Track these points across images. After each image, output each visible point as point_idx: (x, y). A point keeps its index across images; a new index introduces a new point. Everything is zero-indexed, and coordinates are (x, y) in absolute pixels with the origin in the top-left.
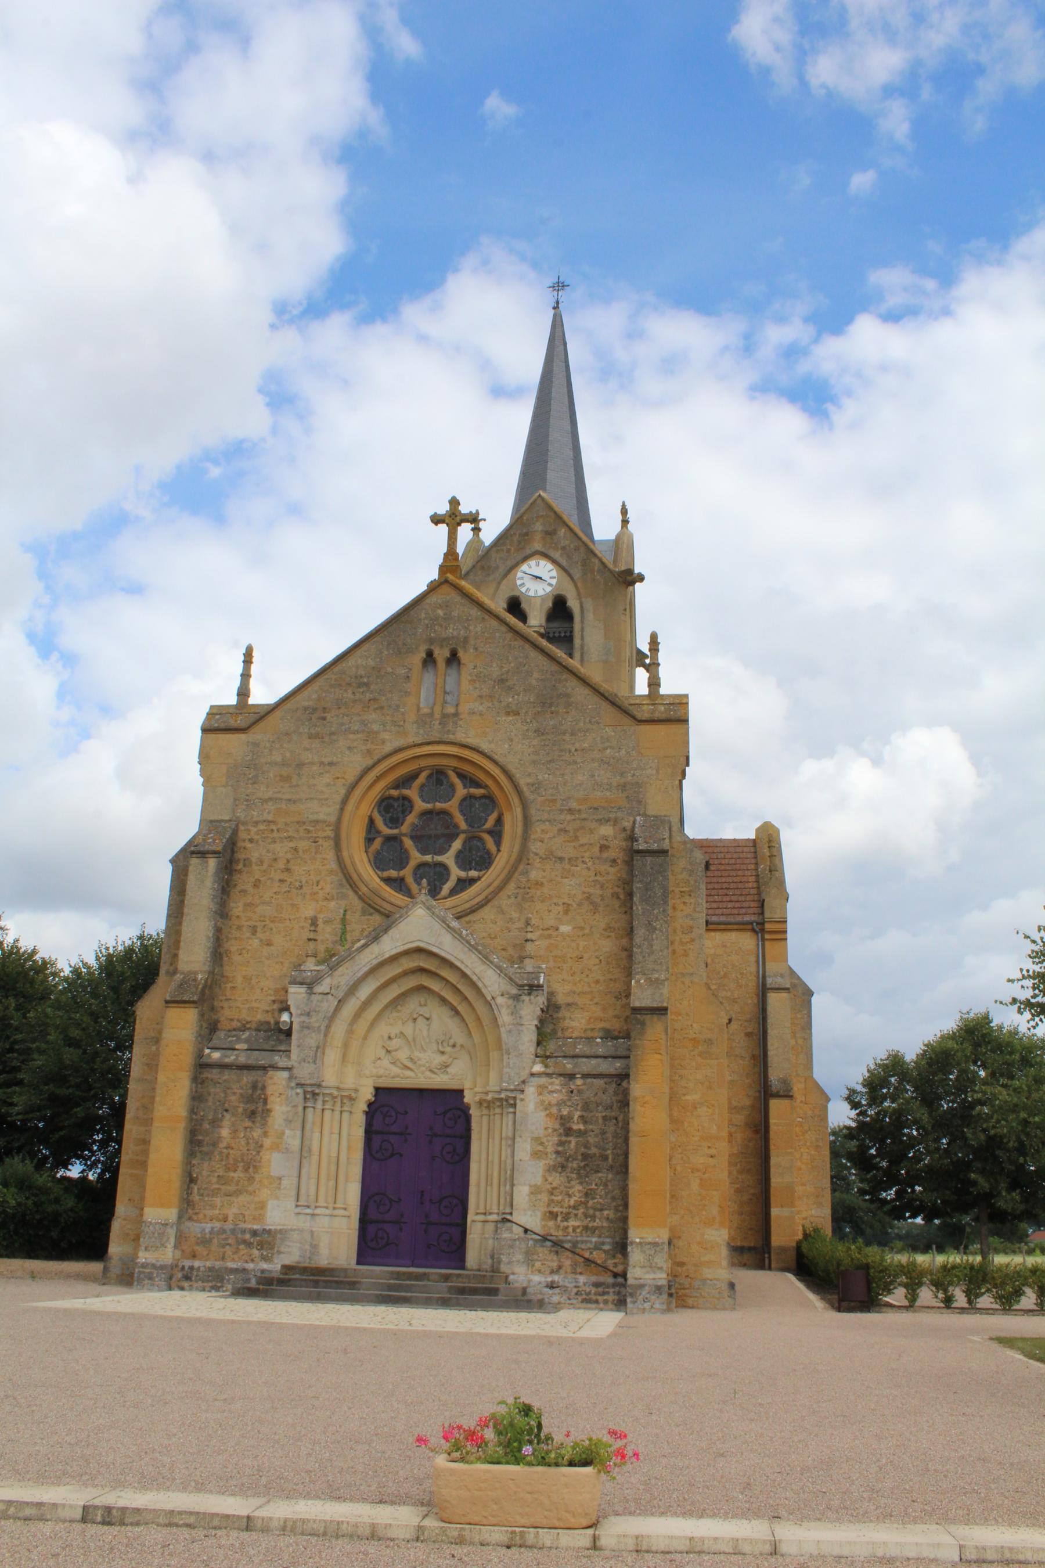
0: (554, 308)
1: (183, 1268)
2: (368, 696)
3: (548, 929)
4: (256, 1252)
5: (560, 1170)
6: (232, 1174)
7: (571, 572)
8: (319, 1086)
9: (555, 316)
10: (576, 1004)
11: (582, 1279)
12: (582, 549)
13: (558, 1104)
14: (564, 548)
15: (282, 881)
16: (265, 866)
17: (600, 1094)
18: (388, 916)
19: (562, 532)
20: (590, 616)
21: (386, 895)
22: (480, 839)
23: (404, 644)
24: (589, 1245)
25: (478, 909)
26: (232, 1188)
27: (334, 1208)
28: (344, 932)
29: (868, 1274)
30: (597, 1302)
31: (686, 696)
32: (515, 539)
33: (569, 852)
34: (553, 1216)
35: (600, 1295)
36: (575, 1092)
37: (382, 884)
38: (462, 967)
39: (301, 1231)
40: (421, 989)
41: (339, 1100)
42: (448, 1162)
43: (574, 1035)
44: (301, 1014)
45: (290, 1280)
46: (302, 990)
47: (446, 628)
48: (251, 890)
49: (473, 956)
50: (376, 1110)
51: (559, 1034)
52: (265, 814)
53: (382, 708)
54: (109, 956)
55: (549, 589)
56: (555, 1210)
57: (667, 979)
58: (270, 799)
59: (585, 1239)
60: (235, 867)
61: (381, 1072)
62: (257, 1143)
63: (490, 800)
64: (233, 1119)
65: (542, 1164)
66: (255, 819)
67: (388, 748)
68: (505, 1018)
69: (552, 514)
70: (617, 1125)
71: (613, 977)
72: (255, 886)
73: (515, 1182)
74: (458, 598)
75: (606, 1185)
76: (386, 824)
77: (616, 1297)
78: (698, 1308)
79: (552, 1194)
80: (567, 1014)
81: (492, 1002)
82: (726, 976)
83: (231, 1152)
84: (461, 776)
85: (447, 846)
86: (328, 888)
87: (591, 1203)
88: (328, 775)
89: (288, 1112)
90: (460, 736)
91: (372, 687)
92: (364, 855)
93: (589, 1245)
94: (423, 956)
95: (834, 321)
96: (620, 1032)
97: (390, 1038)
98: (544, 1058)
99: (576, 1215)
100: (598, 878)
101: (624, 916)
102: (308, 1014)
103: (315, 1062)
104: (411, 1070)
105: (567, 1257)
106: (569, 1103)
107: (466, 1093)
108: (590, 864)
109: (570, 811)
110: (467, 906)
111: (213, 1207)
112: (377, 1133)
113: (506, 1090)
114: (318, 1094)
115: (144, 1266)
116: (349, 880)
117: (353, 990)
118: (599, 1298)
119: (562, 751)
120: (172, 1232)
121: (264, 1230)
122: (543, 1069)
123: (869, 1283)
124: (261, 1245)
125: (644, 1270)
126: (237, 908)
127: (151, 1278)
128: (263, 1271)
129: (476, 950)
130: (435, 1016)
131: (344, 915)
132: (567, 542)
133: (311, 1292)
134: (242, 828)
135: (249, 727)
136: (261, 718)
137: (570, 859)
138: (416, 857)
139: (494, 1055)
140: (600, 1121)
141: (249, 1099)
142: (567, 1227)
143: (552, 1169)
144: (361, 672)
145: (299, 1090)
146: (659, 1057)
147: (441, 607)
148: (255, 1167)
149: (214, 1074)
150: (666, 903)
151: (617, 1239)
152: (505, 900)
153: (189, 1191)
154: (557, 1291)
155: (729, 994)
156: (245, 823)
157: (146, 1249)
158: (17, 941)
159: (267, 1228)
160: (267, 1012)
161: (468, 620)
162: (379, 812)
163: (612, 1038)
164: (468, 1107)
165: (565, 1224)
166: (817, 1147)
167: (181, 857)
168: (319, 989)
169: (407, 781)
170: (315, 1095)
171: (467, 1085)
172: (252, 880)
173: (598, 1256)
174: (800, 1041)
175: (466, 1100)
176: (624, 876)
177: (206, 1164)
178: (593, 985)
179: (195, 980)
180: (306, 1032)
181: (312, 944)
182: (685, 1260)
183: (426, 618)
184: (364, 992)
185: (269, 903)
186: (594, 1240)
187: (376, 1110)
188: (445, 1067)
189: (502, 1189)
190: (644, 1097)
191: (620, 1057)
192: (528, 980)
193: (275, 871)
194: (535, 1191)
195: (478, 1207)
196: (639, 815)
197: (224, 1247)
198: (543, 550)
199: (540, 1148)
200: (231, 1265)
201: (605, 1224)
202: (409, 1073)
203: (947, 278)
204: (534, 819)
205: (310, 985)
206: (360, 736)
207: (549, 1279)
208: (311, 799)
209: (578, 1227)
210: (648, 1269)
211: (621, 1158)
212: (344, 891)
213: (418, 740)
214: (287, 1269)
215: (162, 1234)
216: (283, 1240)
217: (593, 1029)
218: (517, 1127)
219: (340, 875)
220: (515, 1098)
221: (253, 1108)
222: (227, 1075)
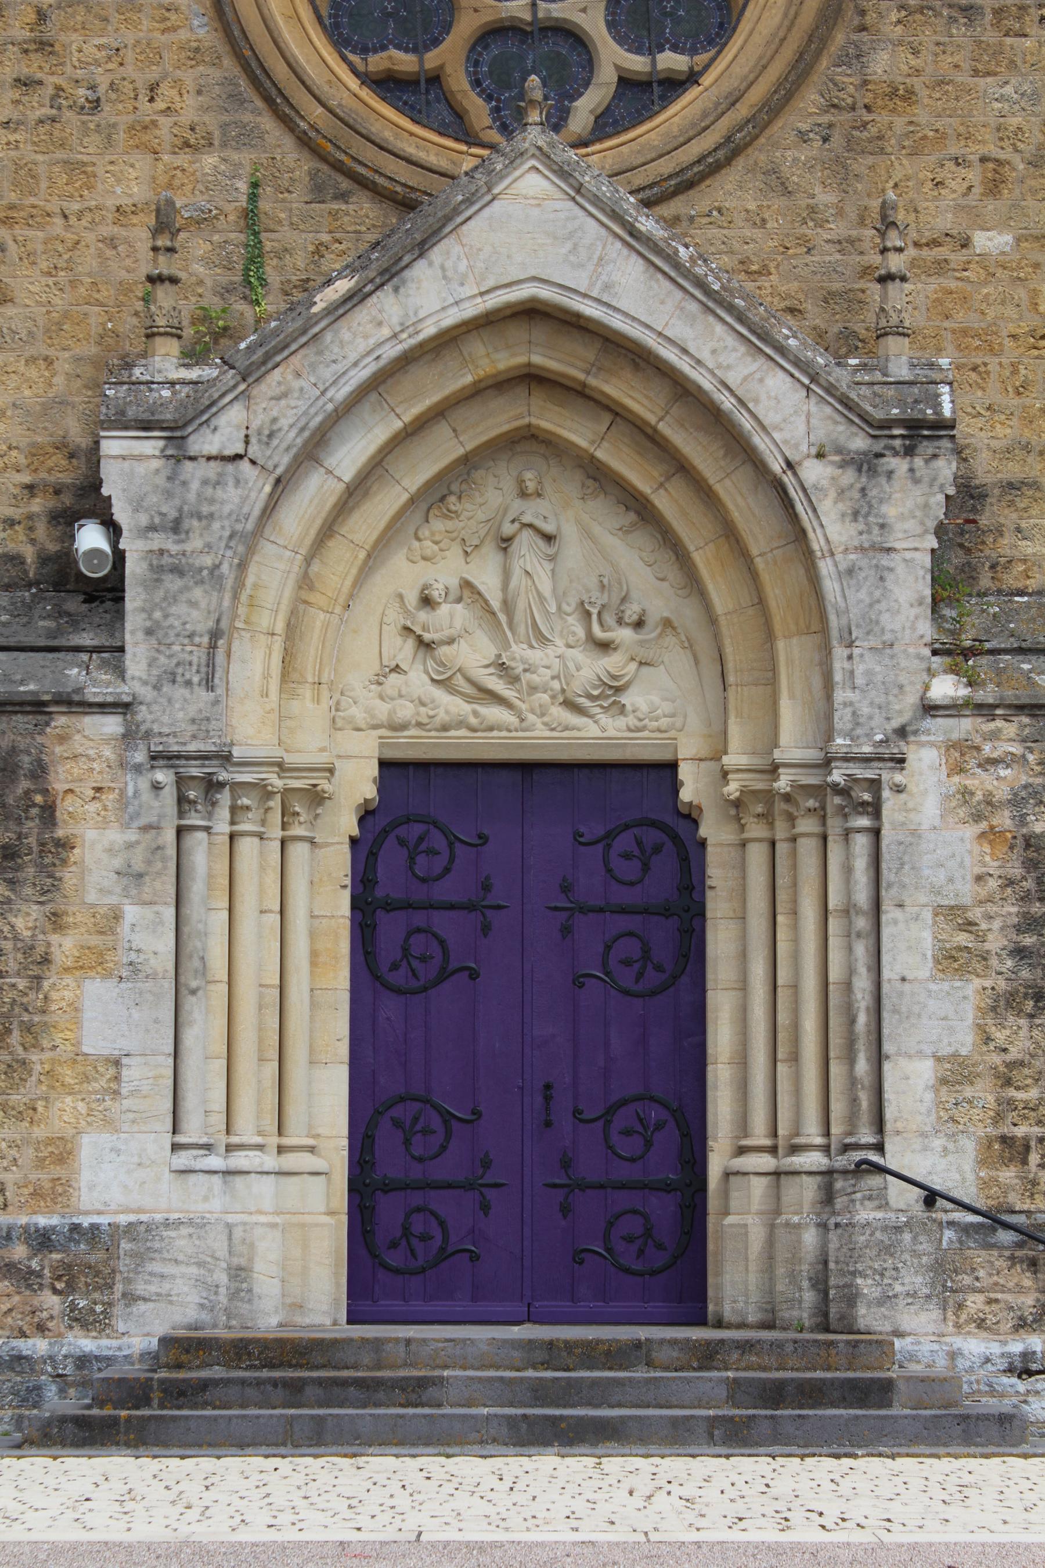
3: (934, 243)
4: (51, 1302)
5: (1029, 1005)
8: (225, 758)
13: (1016, 801)
15: (25, 83)
18: (406, 204)
21: (388, 135)
25: (703, 177)
27: (281, 1150)
28: (255, 258)
34: (1015, 1150)
37: (365, 93)
38: (684, 365)
39: (198, 1225)
41: (276, 803)
42: (626, 993)
43: (1032, 584)
44: (152, 528)
46: (151, 446)
49: (719, 329)
50: (385, 832)
51: (985, 581)
56: (1020, 1131)
61: (406, 711)
65: (971, 992)
68: (832, 527)
73: (888, 1047)
79: (1008, 1082)
80: (1009, 518)
81: (788, 479)
86: (189, 108)
89: (130, 846)
94: (540, 332)
97: (427, 601)
98: (954, 653)
102: (176, 527)
103: (209, 684)
107: (685, 772)
110: (666, 166)
112: (389, 906)
116: (261, 80)
117: (313, 449)
121: (75, 1228)
122: (963, 692)
124: (67, 1279)
128: (83, 1361)
129: (730, 308)
130: (569, 532)
131: (253, 198)
133: (291, 1420)
137: (999, 12)
139: (792, 652)
143: (1003, 1004)
145: (160, 776)
148: (28, 1028)
152: (789, 149)
158: (442, 67)
159: (86, 1221)
164: (691, 818)
170: (212, 786)
171: (688, 748)
175: (686, 795)
180: (172, 583)
181: (165, 296)
184: (350, 455)
187: (385, 832)
188: (613, 690)
189: (836, 1069)
192: (901, 403)
194: (954, 1074)
199: (963, 939)
202: (494, 713)
205: (175, 430)
207: (1016, 1347)
212: (247, 117)
214: (182, 1348)
216: (140, 1258)
218: (887, 875)
219: (228, 62)
220: (875, 785)
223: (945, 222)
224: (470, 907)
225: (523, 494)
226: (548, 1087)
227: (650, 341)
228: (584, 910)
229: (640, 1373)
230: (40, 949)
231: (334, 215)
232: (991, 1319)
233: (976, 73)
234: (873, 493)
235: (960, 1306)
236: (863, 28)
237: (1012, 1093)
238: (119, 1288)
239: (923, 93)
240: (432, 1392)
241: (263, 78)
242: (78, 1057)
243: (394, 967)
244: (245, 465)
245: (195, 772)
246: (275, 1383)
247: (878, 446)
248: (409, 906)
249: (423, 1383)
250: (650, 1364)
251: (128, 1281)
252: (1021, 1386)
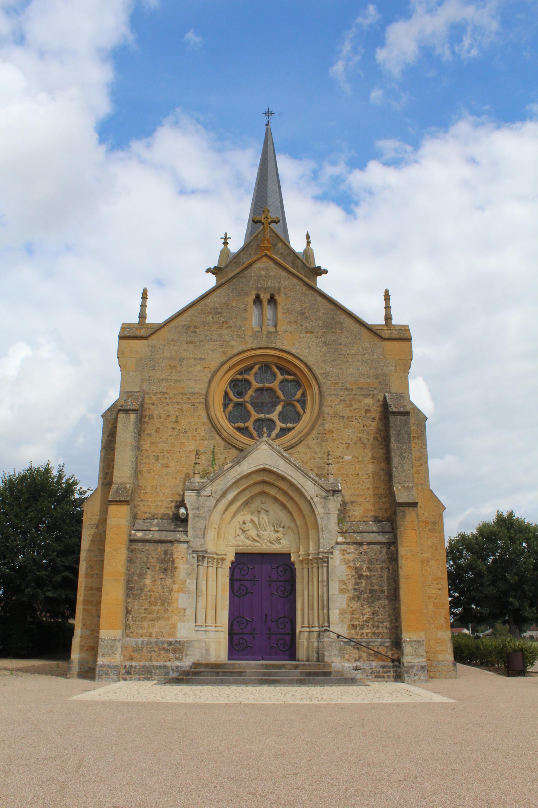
0: (266, 125)
1: (125, 666)
2: (222, 319)
3: (337, 458)
4: (171, 655)
6: (154, 607)
8: (206, 552)
9: (267, 129)
10: (356, 502)
11: (374, 664)
12: (292, 255)
13: (354, 561)
14: (281, 254)
15: (173, 428)
16: (162, 419)
17: (378, 554)
18: (241, 450)
19: (280, 245)
22: (293, 406)
23: (242, 290)
24: (376, 643)
26: (154, 616)
28: (214, 460)
29: (523, 654)
30: (383, 677)
31: (408, 326)
33: (347, 413)
34: (354, 627)
35: (385, 673)
36: (363, 553)
37: (235, 431)
38: (292, 480)
40: (263, 493)
41: (215, 560)
43: (356, 520)
44: (194, 509)
45: (200, 672)
46: (194, 494)
47: (267, 282)
48: (154, 434)
49: (298, 473)
50: (236, 566)
51: (347, 520)
52: (161, 387)
53: (231, 327)
54: (11, 481)
56: (355, 623)
57: (413, 487)
58: (164, 379)
59: (374, 640)
60: (143, 420)
61: (240, 543)
62: (169, 588)
63: (298, 383)
64: (153, 573)
65: (346, 596)
66: (155, 391)
67: (235, 351)
68: (319, 510)
70: (388, 572)
71: (376, 486)
72: (157, 431)
73: (330, 607)
74: (273, 265)
75: (384, 608)
76: (235, 396)
77: (395, 674)
78: (436, 678)
79: (353, 614)
80: (352, 508)
81: (311, 501)
83: (152, 594)
84: (280, 368)
85: (272, 409)
86: (203, 433)
87: (376, 619)
88: (199, 366)
89: (188, 568)
90: (279, 345)
91: (224, 315)
92: (223, 414)
93: (376, 643)
94: (266, 473)
95: (359, 163)
96: (383, 518)
98: (342, 533)
99: (368, 626)
100: (365, 428)
101: (381, 451)
102: (198, 509)
103: (204, 538)
104: (258, 542)
105: (364, 651)
106: (360, 560)
107: (292, 555)
108: (360, 420)
109: (347, 390)
110: (289, 444)
111: (142, 628)
112: (236, 580)
113: (322, 553)
114: (205, 557)
115: (102, 666)
117: (224, 495)
118: (385, 675)
119: (339, 354)
120: (119, 645)
121: (176, 641)
122: (344, 540)
123: (523, 659)
124: (175, 651)
125: (413, 657)
126: (146, 444)
127: (106, 674)
128: (177, 667)
129: (300, 469)
131: (214, 449)
132: (283, 251)
134: (147, 396)
135: (149, 336)
136: (156, 331)
137: (348, 417)
138: (255, 415)
139: (312, 532)
140: (379, 570)
141: (163, 561)
142: (363, 633)
143: (352, 599)
144: (217, 305)
145: (195, 555)
146: (414, 531)
147: (263, 269)
148: (168, 603)
149: (139, 546)
150: (410, 442)
151: (393, 640)
152: (311, 441)
153: (127, 619)
154: (359, 671)
156: (148, 394)
157: (103, 655)
159: (178, 640)
160: (168, 508)
161: (279, 278)
162: (230, 388)
163: (378, 522)
164: (293, 564)
165: (362, 631)
167: (109, 414)
168: (204, 493)
169: (248, 369)
170: (204, 557)
172: (155, 427)
173: (383, 650)
175: (292, 559)
176: (380, 427)
177: (136, 602)
178: (366, 491)
179: (126, 488)
180: (197, 519)
183: (254, 276)
184: (230, 496)
185: (165, 442)
186: (379, 640)
187: (236, 566)
188: (278, 540)
190: (407, 555)
191: (386, 532)
192: (332, 487)
193: (169, 422)
194: (343, 612)
195: (303, 622)
196: (387, 392)
197: (150, 653)
199: (344, 587)
200: (158, 664)
201: (385, 631)
203: (416, 145)
204: (326, 394)
205: (198, 491)
206: (218, 343)
207: (355, 665)
208: (190, 379)
209: (369, 633)
210: (415, 656)
211: (393, 591)
213: (254, 346)
214: (196, 665)
215: (112, 646)
217: (367, 516)
218: (330, 575)
220: (327, 558)
221: (165, 566)
222: (148, 546)
224: (252, 581)
225: (262, 503)
226: (266, 615)
227: (286, 475)
228: (273, 581)
229: (283, 670)
230: (171, 588)
231: (228, 452)
232: (350, 659)
233: (344, 428)
234: (327, 503)
235: (344, 657)
236: (324, 420)
237: (354, 616)
238: (184, 653)
239: (334, 431)
240: (243, 674)
242: (178, 608)
243: (237, 592)
244: (211, 497)
245: (201, 554)
246: (214, 672)
247: (328, 495)
248: (240, 580)
249: (242, 672)
250: (285, 668)
251: (186, 652)
252: (356, 672)
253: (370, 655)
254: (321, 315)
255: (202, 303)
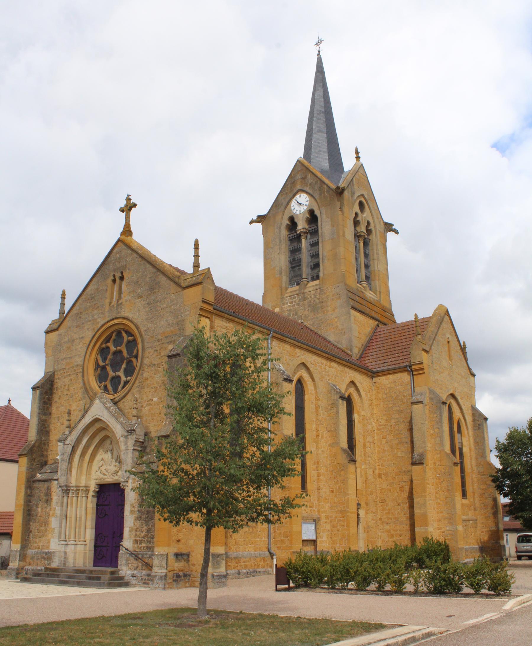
2: (94, 302)
7: (314, 196)
12: (319, 182)
14: (310, 184)
15: (67, 395)
19: (309, 176)
20: (324, 216)
32: (289, 186)
39: (60, 552)
46: (62, 444)
48: (58, 401)
55: (305, 208)
69: (304, 168)
82: (396, 398)
84: (126, 332)
87: (149, 535)
109: (159, 340)
111: (36, 542)
142: (141, 547)
145: (60, 489)
154: (135, 578)
155: (398, 408)
165: (141, 545)
166: (448, 490)
174: (436, 430)
182: (195, 563)
189: (77, 530)
198: (302, 188)
199: (133, 509)
202: (106, 477)
223: (150, 397)
241: (340, 361)
250: (86, 573)
253: (143, 565)
254: (148, 280)
255: (85, 293)
